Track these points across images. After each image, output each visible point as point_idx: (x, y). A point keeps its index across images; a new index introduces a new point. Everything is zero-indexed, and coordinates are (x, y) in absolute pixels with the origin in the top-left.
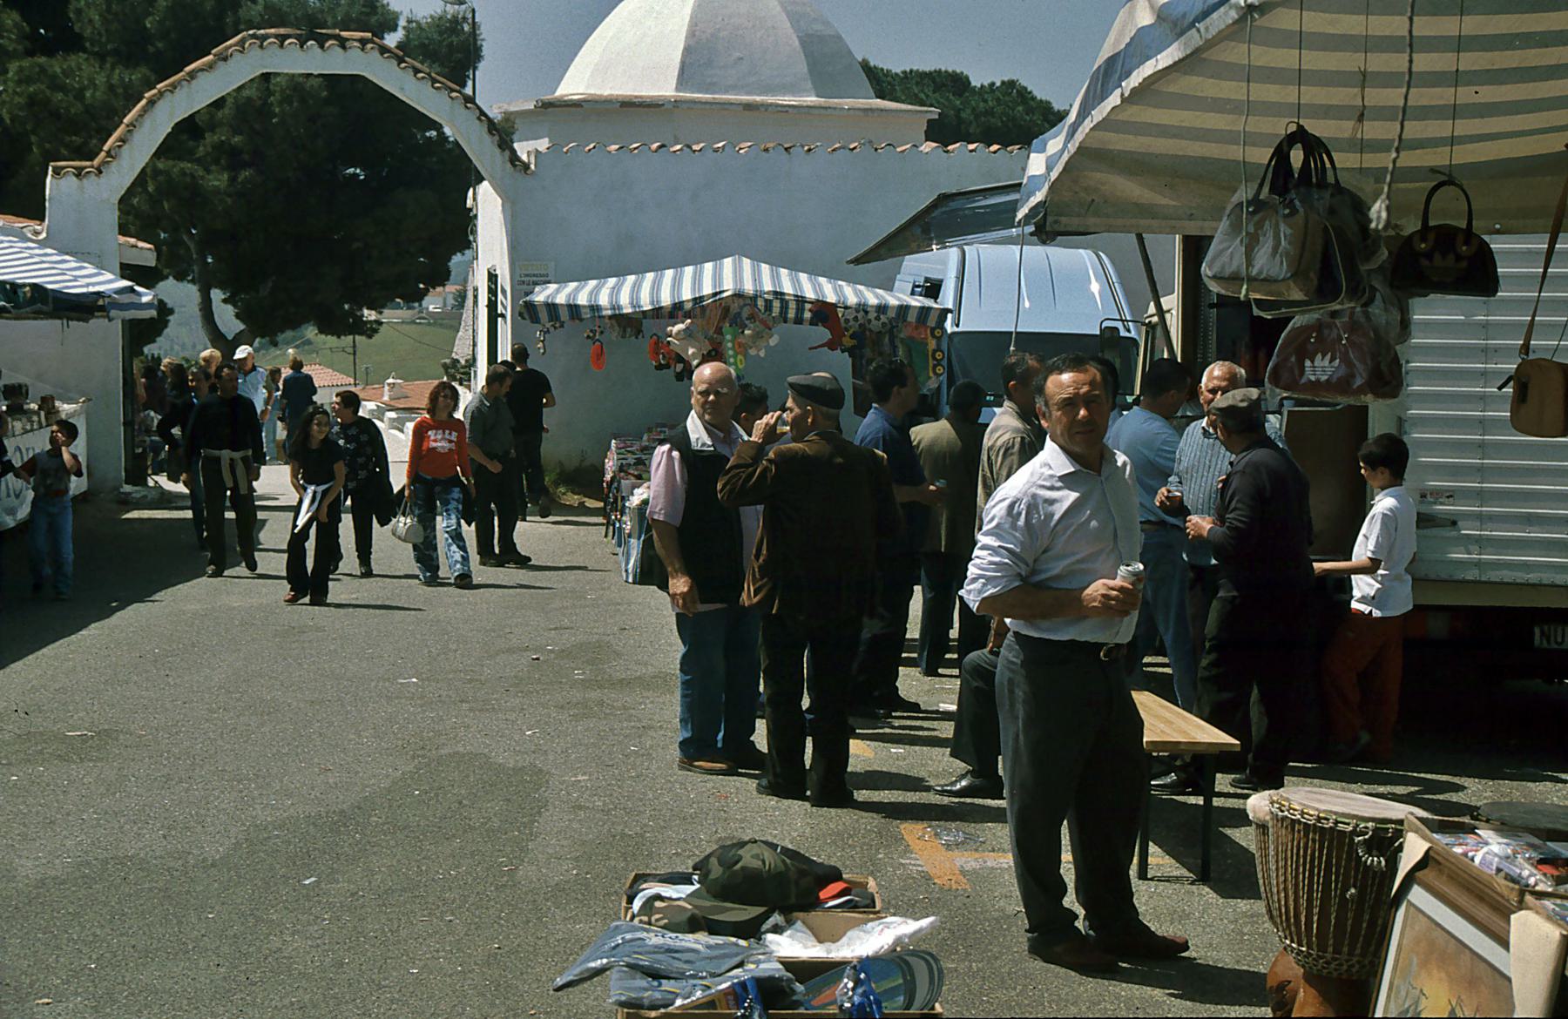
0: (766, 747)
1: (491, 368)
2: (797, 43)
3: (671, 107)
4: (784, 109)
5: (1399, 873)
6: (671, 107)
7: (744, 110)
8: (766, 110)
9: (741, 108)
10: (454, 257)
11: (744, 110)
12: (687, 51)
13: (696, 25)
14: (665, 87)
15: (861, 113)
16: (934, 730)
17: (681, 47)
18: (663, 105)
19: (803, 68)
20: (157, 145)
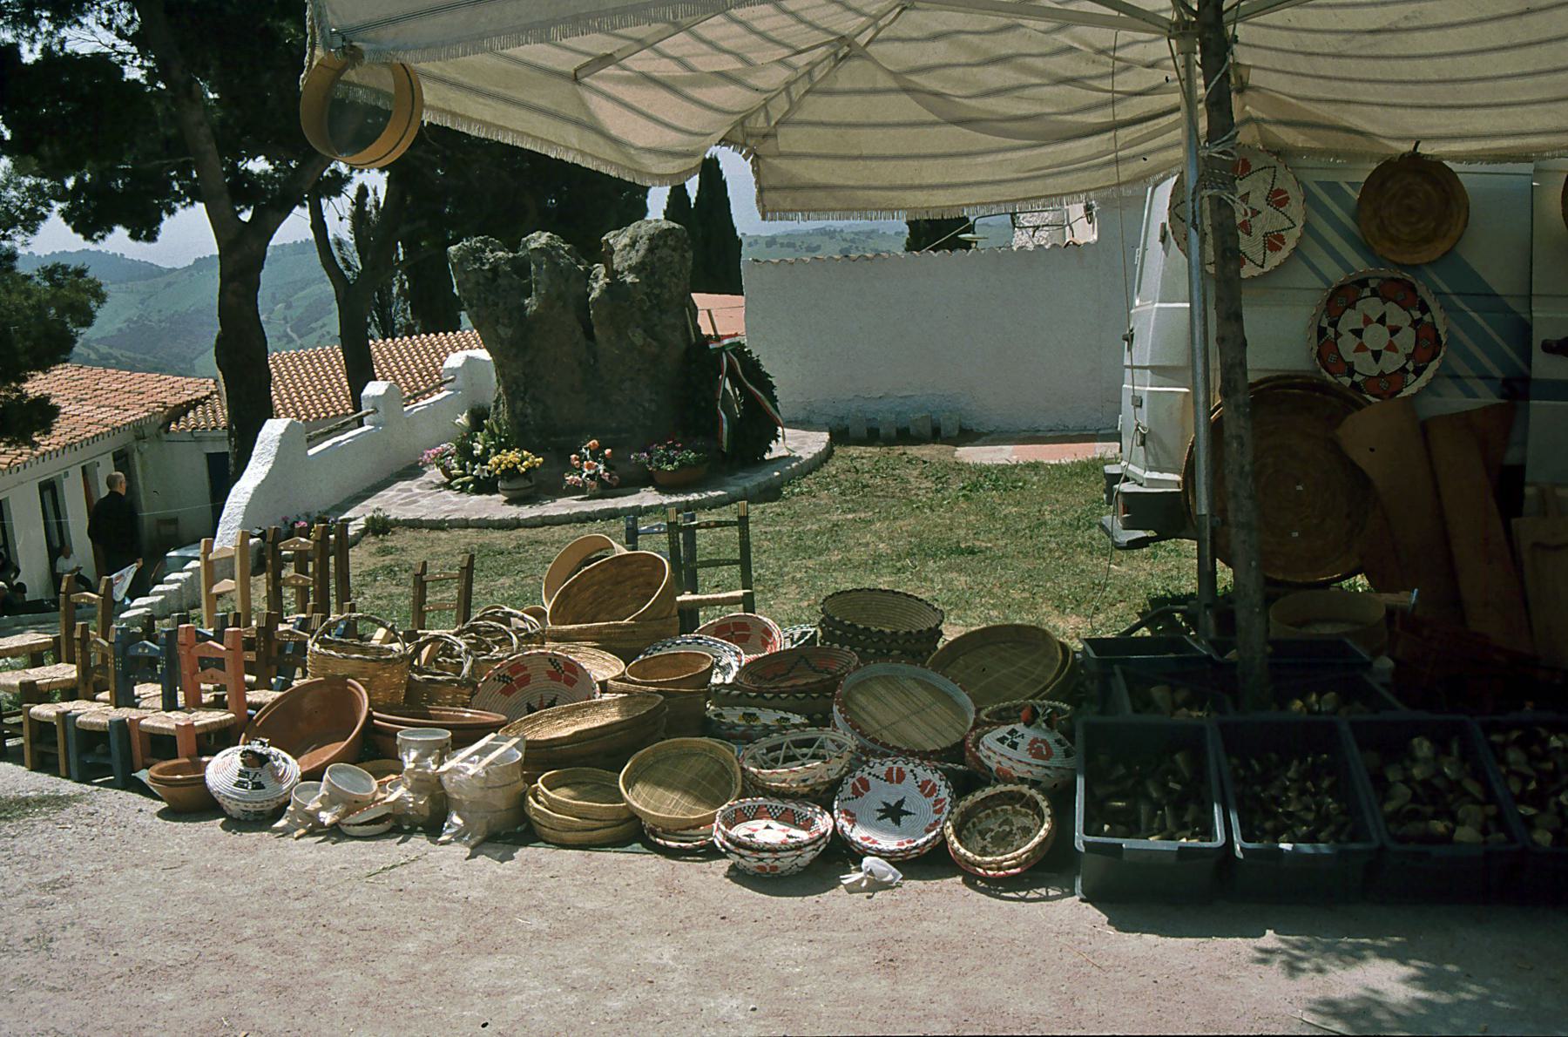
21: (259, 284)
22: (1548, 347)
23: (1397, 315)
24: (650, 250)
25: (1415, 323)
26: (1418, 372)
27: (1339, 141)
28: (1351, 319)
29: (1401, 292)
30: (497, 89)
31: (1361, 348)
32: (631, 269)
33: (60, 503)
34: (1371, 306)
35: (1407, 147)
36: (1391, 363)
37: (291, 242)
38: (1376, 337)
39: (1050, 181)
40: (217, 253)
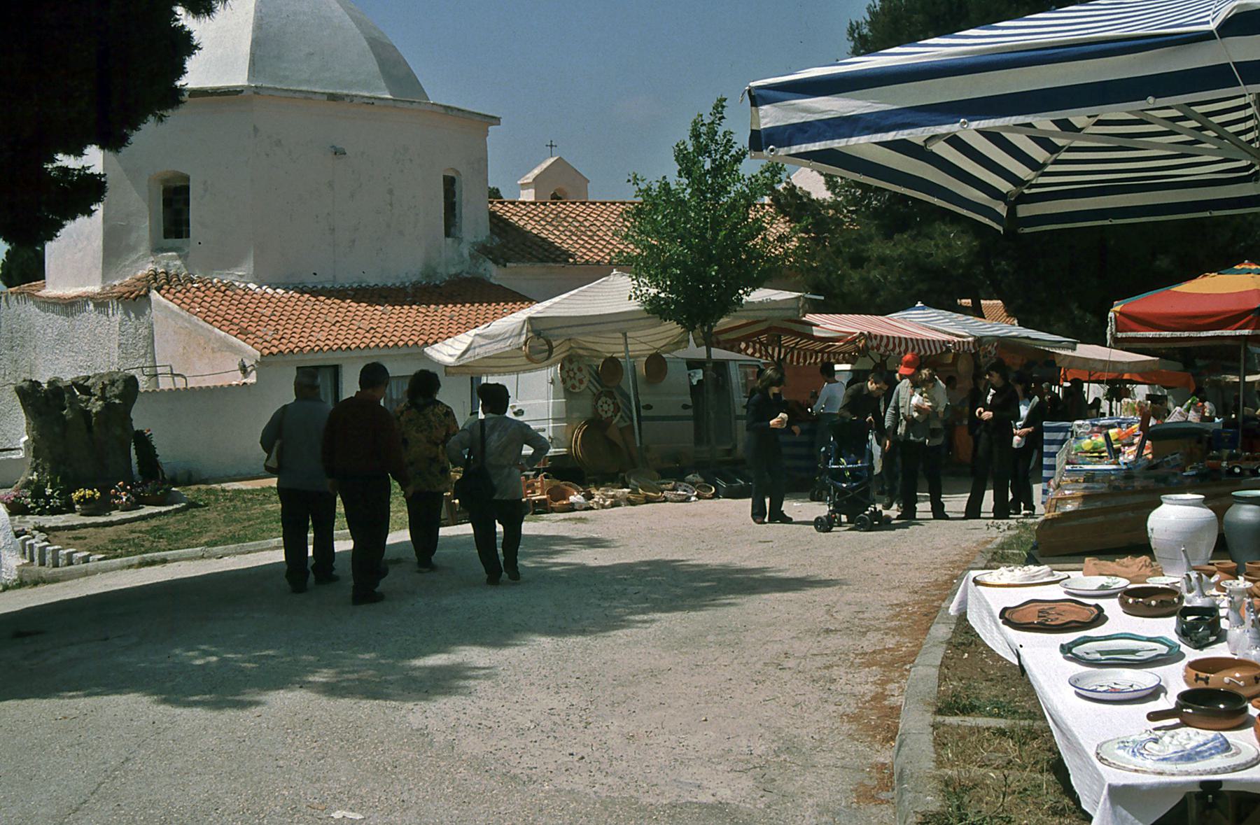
0: (392, 542)
1: (1039, 560)
2: (365, 44)
3: (250, 93)
4: (371, 101)
5: (1088, 631)
6: (250, 93)
7: (328, 99)
8: (352, 101)
9: (326, 97)
10: (998, 375)
11: (328, 99)
12: (256, 43)
13: (262, 19)
14: (240, 78)
15: (443, 111)
16: (1155, 729)
17: (250, 39)
18: (242, 91)
19: (374, 67)
20: (918, 83)
21: (360, 383)
22: (643, 407)
23: (610, 401)
24: (125, 387)
25: (613, 403)
26: (616, 416)
27: (595, 353)
28: (600, 403)
29: (610, 395)
30: (84, 289)
31: (603, 410)
32: (116, 396)
33: (1072, 43)
34: (603, 399)
35: (609, 355)
36: (610, 414)
37: (136, 137)
38: (605, 407)
39: (638, 349)
40: (335, 542)
